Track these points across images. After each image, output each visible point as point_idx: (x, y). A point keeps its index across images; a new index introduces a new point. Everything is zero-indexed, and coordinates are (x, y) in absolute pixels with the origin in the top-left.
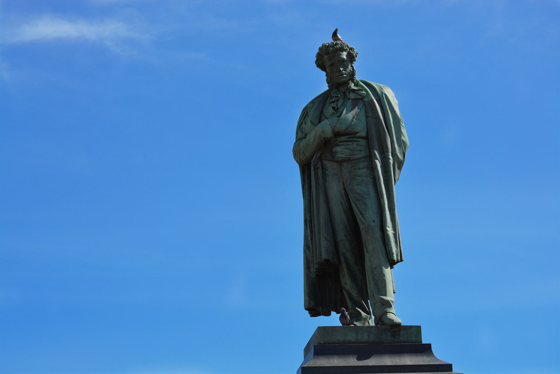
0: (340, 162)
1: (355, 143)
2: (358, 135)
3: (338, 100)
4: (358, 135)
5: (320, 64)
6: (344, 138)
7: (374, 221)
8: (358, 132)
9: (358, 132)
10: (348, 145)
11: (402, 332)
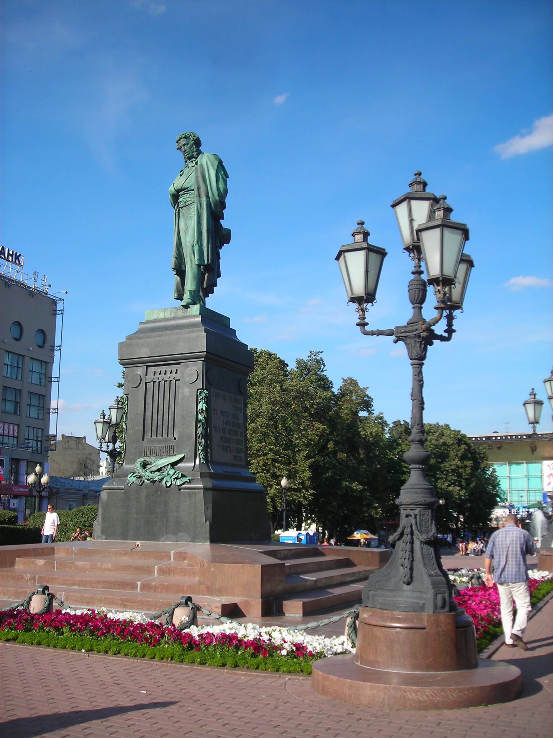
6: (182, 192)
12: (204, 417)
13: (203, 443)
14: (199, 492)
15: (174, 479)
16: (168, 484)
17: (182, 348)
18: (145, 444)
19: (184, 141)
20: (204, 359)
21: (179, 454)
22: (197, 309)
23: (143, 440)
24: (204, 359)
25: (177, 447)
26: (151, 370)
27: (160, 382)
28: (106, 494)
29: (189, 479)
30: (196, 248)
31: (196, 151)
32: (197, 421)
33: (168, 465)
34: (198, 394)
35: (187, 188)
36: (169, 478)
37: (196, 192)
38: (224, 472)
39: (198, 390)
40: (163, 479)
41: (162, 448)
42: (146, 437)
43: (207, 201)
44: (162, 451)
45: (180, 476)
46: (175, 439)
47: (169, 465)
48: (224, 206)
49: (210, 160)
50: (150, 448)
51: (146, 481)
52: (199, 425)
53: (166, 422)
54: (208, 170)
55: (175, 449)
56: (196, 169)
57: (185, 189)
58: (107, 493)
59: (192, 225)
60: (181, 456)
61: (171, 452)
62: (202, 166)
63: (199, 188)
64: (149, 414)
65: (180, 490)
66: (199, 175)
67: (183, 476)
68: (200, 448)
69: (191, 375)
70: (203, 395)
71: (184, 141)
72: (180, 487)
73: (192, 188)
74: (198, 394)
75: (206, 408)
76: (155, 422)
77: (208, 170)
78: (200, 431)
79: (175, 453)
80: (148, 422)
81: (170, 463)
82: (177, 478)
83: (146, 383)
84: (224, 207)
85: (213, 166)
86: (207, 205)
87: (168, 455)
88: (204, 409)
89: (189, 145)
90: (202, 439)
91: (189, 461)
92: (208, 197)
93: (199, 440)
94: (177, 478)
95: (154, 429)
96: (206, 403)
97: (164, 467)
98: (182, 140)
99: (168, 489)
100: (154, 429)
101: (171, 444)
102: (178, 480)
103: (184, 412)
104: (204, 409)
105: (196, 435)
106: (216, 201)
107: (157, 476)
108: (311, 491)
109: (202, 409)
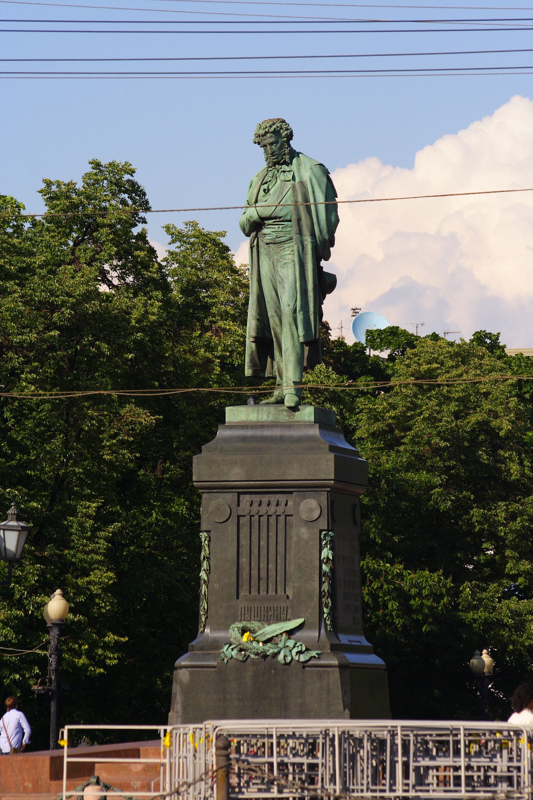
1: (281, 226)
6: (271, 222)
12: (331, 569)
13: (330, 605)
14: (333, 671)
15: (297, 653)
16: (289, 659)
17: (295, 472)
18: (242, 604)
19: (271, 137)
20: (329, 489)
21: (295, 618)
22: (310, 414)
23: (238, 598)
24: (329, 489)
25: (292, 608)
26: (246, 499)
27: (260, 516)
28: (187, 674)
29: (317, 654)
30: (300, 317)
31: (288, 154)
32: (321, 574)
33: (282, 634)
34: (322, 536)
35: (280, 218)
36: (289, 651)
37: (294, 223)
38: (349, 641)
39: (321, 531)
40: (279, 652)
41: (268, 609)
42: (242, 594)
43: (312, 243)
44: (270, 613)
45: (304, 649)
46: (288, 597)
47: (284, 635)
48: (332, 242)
49: (315, 176)
50: (250, 609)
51: (252, 656)
52: (323, 579)
53: (272, 573)
54: (314, 192)
55: (289, 612)
56: (294, 187)
57: (276, 218)
58: (190, 672)
59: (291, 278)
60: (300, 621)
61: (282, 616)
62: (302, 183)
63: (299, 220)
64: (244, 560)
65: (304, 667)
66: (300, 199)
67: (307, 650)
68: (325, 610)
69: (311, 510)
70: (328, 538)
71: (271, 137)
72: (305, 665)
73: (288, 218)
74: (322, 536)
75: (333, 556)
76: (255, 572)
77: (314, 192)
78: (326, 587)
79: (288, 617)
80: (245, 574)
81: (286, 632)
82: (300, 653)
83: (239, 517)
84: (332, 245)
85: (320, 185)
86: (312, 248)
87: (278, 620)
88: (331, 558)
89: (279, 145)
90: (327, 598)
91: (311, 628)
92: (313, 234)
93: (324, 600)
94: (300, 653)
95: (255, 582)
96: (331, 549)
97: (277, 636)
98: (268, 135)
99: (286, 667)
100: (255, 582)
101: (283, 604)
102: (301, 656)
103: (301, 561)
104: (331, 558)
105: (320, 593)
106: (324, 239)
107: (270, 649)
108: (83, 600)
109: (328, 557)
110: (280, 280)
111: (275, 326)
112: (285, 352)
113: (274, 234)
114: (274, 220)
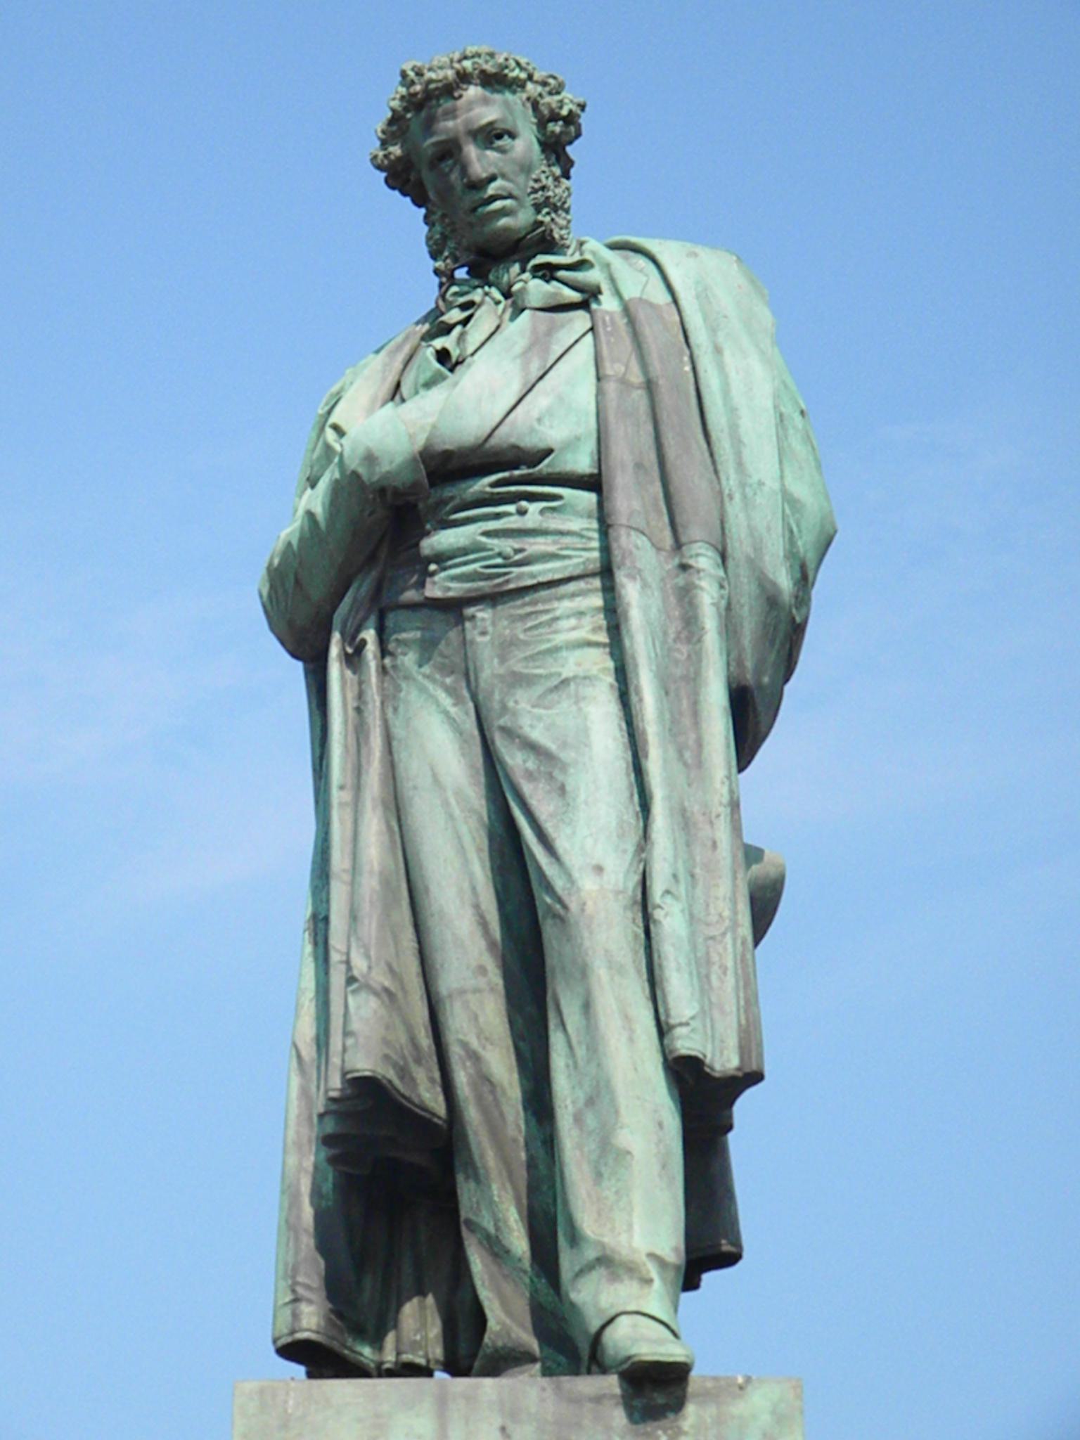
0: (453, 609)
1: (534, 508)
2: (544, 467)
3: (465, 322)
4: (544, 467)
5: (401, 176)
6: (483, 484)
7: (599, 869)
8: (549, 452)
9: (549, 452)
10: (498, 516)
11: (690, 1409)
110: (531, 764)
111: (475, 1044)
112: (578, 1119)
113: (507, 545)
114: (506, 474)
